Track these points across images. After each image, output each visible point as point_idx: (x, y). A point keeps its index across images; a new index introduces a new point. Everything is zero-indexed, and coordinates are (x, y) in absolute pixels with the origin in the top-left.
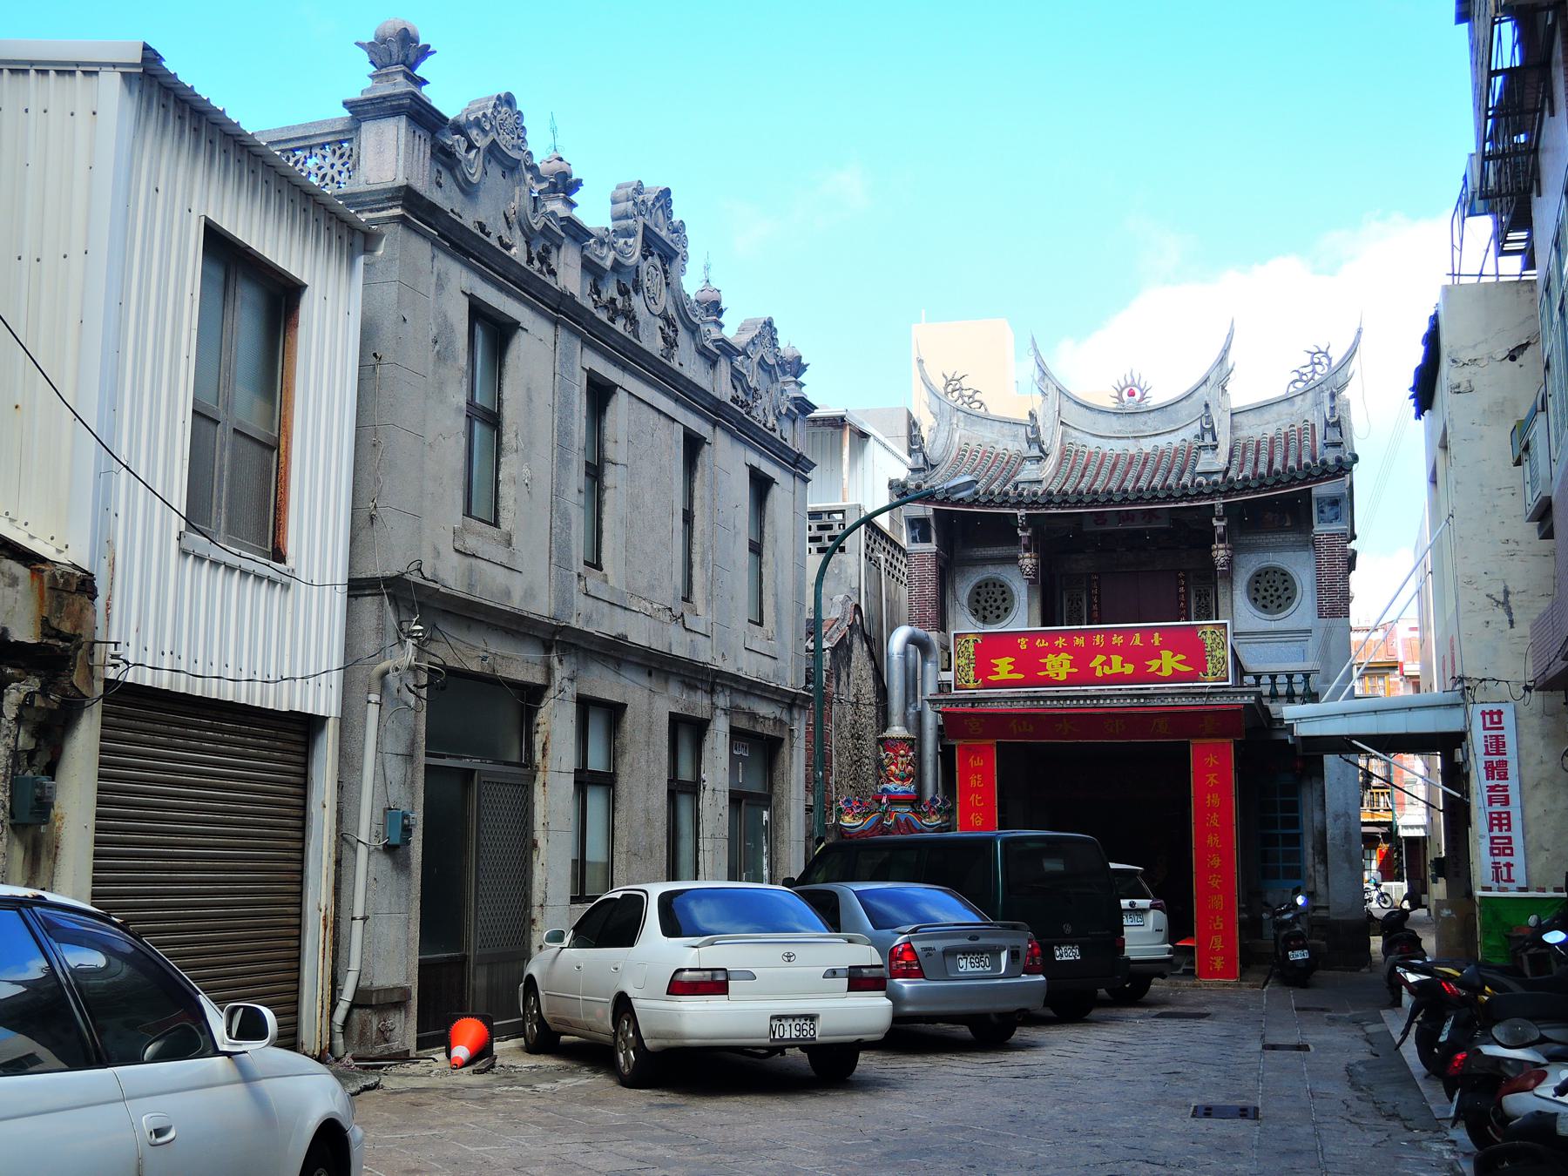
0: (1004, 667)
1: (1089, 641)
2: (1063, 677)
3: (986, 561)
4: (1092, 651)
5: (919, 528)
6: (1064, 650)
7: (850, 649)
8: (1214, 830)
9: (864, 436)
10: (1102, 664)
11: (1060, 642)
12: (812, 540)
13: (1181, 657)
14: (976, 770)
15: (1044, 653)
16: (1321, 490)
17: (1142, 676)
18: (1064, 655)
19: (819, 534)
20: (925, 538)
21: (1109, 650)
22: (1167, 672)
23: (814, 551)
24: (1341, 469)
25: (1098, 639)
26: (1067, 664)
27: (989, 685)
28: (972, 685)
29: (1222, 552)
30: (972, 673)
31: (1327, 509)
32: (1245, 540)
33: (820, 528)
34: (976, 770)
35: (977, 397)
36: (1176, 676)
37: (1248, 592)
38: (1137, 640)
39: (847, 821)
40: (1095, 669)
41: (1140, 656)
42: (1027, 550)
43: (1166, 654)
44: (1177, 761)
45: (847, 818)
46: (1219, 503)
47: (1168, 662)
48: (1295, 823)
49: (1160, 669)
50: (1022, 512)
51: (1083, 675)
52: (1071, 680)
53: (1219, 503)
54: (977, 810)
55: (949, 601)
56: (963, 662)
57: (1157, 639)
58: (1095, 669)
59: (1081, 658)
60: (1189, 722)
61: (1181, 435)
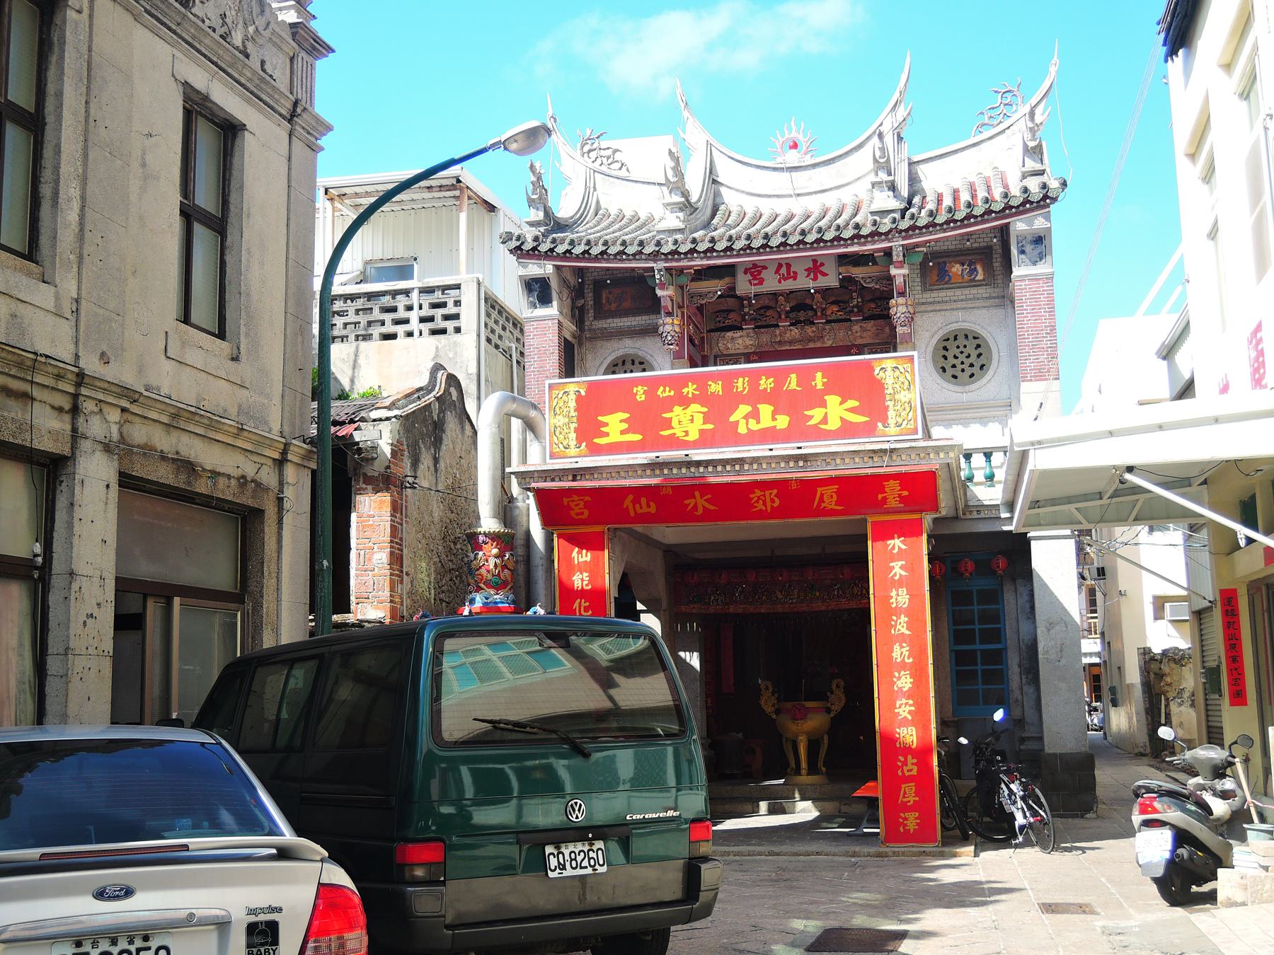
0: (615, 425)
2: (693, 436)
3: (622, 333)
4: (731, 400)
5: (538, 290)
6: (695, 399)
10: (746, 417)
11: (690, 390)
13: (852, 403)
15: (668, 404)
16: (1019, 226)
17: (799, 430)
20: (545, 300)
21: (755, 397)
22: (833, 424)
24: (1045, 197)
25: (741, 384)
26: (699, 418)
27: (595, 450)
29: (902, 309)
30: (573, 435)
33: (435, 306)
35: (618, 156)
36: (847, 430)
37: (935, 361)
38: (793, 382)
41: (796, 405)
43: (833, 400)
44: (853, 565)
47: (836, 410)
48: (996, 636)
49: (825, 420)
50: (662, 265)
51: (721, 432)
52: (705, 440)
53: (897, 244)
56: (560, 420)
57: (819, 381)
59: (718, 410)
60: (860, 491)
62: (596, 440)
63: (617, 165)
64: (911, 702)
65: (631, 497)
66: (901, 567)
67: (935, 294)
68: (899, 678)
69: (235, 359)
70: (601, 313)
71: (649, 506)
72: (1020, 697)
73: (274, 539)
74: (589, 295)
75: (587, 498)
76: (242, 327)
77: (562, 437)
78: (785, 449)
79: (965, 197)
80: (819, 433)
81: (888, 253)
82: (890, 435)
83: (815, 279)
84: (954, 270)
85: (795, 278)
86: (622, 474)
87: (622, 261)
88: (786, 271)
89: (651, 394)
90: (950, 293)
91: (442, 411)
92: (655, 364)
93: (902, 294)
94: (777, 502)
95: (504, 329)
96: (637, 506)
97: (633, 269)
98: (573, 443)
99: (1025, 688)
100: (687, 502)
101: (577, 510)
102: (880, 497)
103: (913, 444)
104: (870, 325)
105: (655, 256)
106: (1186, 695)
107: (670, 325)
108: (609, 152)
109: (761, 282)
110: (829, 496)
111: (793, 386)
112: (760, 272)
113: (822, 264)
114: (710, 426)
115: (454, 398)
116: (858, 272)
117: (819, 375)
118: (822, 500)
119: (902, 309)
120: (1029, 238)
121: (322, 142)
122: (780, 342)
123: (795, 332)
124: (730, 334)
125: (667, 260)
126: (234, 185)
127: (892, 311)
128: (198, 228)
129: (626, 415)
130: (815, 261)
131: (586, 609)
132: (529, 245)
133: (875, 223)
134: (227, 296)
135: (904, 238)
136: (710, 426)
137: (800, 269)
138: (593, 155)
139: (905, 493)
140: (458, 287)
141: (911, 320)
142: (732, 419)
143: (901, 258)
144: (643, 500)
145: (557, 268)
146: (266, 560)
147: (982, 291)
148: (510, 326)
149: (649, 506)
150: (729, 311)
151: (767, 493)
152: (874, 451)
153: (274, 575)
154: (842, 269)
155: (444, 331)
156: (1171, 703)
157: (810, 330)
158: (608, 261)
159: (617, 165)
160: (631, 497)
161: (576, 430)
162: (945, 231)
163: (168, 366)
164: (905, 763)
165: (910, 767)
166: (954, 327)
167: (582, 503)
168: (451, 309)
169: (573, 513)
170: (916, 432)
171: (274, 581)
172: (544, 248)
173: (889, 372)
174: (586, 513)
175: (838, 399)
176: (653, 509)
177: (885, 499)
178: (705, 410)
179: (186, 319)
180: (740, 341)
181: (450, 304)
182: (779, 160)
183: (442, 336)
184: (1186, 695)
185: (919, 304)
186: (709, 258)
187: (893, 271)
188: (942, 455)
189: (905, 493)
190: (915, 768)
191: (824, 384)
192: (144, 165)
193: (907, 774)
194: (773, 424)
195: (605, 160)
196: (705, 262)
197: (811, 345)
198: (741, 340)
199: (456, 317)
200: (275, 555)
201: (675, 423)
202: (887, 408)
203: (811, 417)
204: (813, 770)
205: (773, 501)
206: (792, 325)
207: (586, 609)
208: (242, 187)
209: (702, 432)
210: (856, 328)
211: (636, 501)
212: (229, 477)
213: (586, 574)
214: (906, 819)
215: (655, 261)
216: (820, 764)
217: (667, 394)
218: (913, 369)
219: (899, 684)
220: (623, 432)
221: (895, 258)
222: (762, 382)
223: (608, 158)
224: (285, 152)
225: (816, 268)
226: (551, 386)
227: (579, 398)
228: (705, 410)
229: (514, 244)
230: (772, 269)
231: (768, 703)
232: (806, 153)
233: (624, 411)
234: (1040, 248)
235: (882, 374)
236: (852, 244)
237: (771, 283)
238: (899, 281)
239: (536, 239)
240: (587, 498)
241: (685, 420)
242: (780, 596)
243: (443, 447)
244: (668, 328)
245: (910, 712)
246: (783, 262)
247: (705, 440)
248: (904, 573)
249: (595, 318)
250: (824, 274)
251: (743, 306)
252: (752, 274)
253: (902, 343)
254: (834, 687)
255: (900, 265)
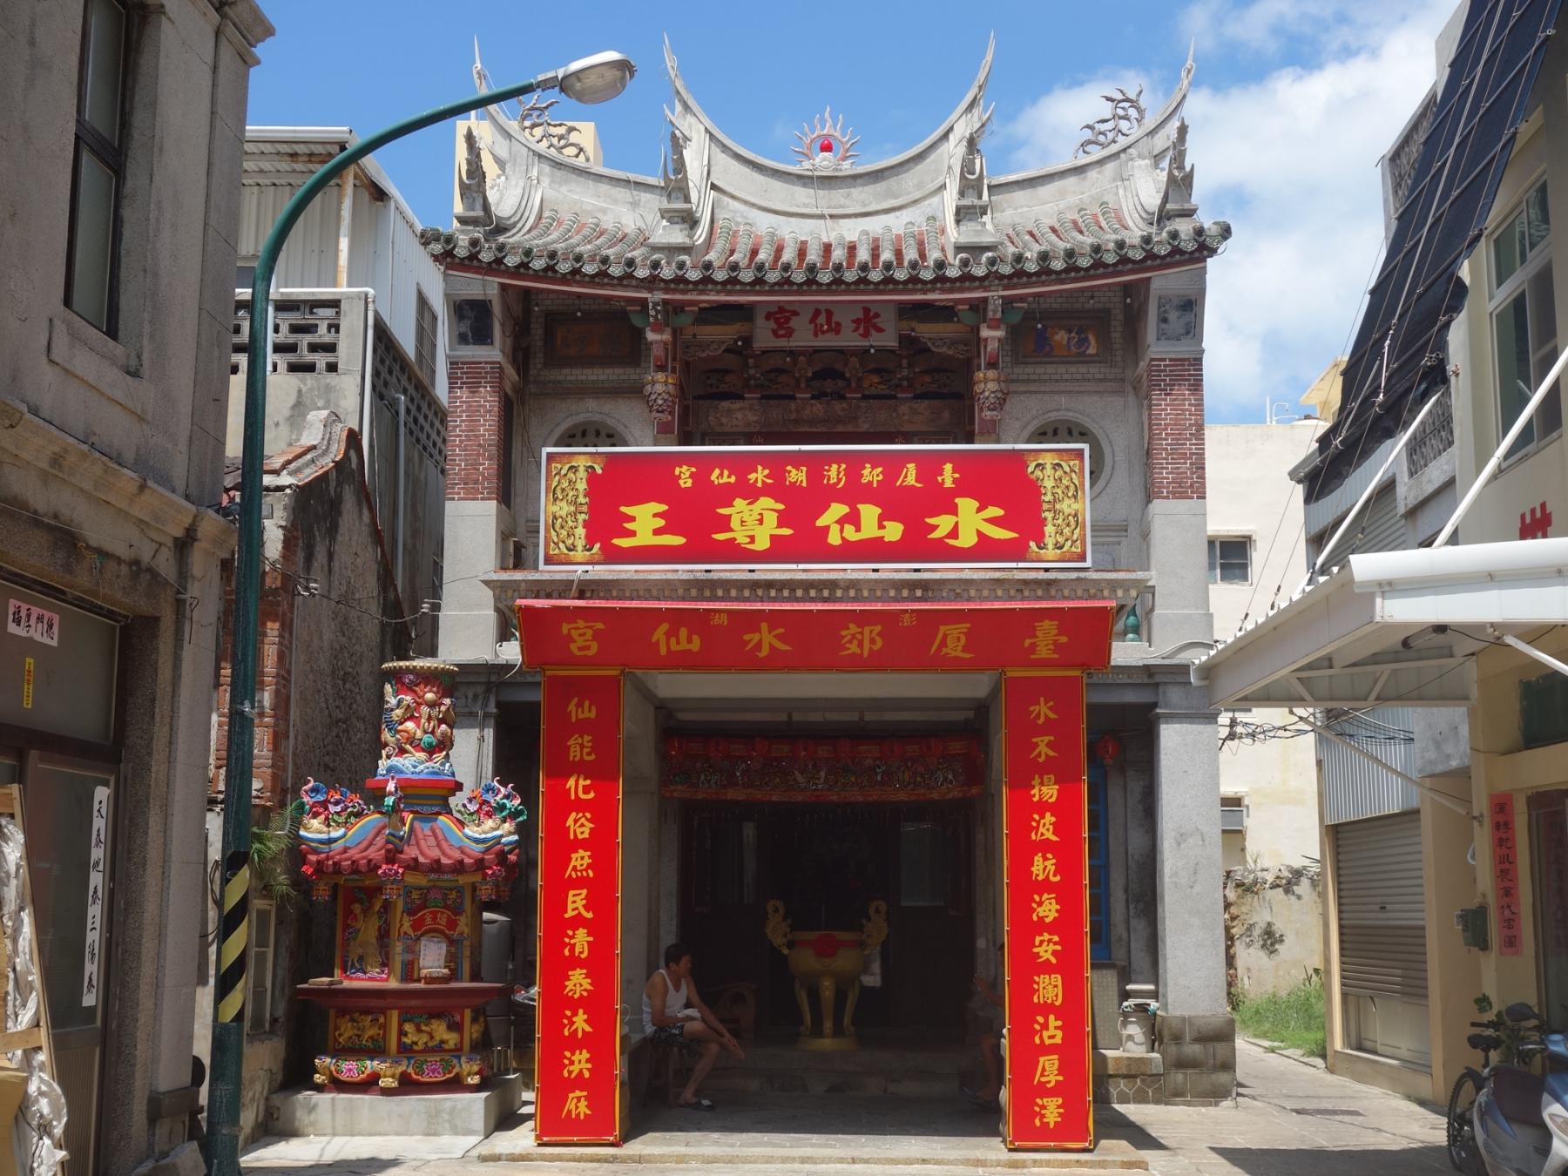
0: (645, 521)
1: (816, 474)
2: (762, 544)
4: (820, 496)
6: (766, 491)
7: (335, 506)
8: (1045, 847)
9: (380, 195)
10: (841, 522)
11: (759, 476)
12: (278, 348)
13: (995, 512)
14: (583, 727)
15: (727, 495)
16: (1164, 283)
17: (918, 545)
18: (766, 502)
19: (292, 338)
20: (480, 335)
21: (854, 494)
22: (967, 540)
23: (282, 367)
25: (834, 473)
26: (771, 519)
27: (614, 556)
28: (580, 554)
29: (992, 386)
30: (581, 531)
31: (1173, 316)
32: (1022, 371)
33: (295, 329)
34: (583, 727)
35: (573, 137)
36: (985, 549)
38: (910, 476)
39: (314, 829)
40: (826, 529)
41: (915, 508)
42: (661, 368)
43: (967, 505)
45: (315, 823)
46: (995, 295)
47: (970, 521)
49: (954, 533)
50: (659, 296)
51: (802, 541)
52: (779, 551)
53: (995, 295)
54: (580, 806)
55: (515, 456)
56: (563, 508)
57: (948, 476)
58: (826, 529)
59: (800, 509)
61: (905, 216)
62: (616, 541)
63: (572, 151)
64: (1056, 938)
65: (665, 627)
66: (1049, 745)
67: (1029, 370)
68: (1040, 904)
69: (134, 374)
70: (555, 359)
71: (689, 641)
72: (1125, 935)
73: (169, 665)
74: (537, 331)
75: (600, 626)
76: (146, 324)
77: (564, 533)
78: (897, 571)
79: (911, 254)
80: (944, 551)
81: (979, 307)
82: (1045, 561)
83: (866, 335)
84: (1057, 337)
85: (837, 332)
86: (733, 593)
87: (602, 286)
88: (825, 318)
89: (701, 478)
90: (1050, 369)
91: (339, 484)
92: (629, 438)
93: (992, 365)
94: (879, 643)
95: (390, 372)
96: (673, 641)
97: (609, 298)
98: (580, 544)
99: (1134, 922)
100: (747, 637)
101: (580, 642)
102: (1027, 642)
103: (1082, 575)
104: (923, 406)
105: (652, 282)
106: (1257, 932)
107: (661, 385)
108: (562, 130)
109: (790, 333)
110: (954, 639)
111: (911, 479)
112: (788, 320)
113: (877, 315)
114: (787, 532)
115: (354, 465)
116: (926, 331)
117: (948, 467)
118: (943, 643)
119: (992, 386)
120: (1175, 302)
121: (260, 50)
122: (797, 422)
123: (818, 408)
124: (725, 404)
125: (666, 291)
126: (140, 98)
127: (978, 388)
128: (86, 157)
129: (663, 508)
130: (866, 310)
131: (586, 790)
132: (461, 252)
133: (965, 263)
134: (123, 274)
135: (1006, 288)
136: (787, 532)
137: (845, 318)
138: (538, 132)
139: (1064, 639)
140: (335, 304)
141: (1000, 403)
142: (820, 522)
143: (999, 315)
144: (683, 632)
145: (503, 287)
146: (159, 696)
147: (1094, 370)
148: (396, 368)
149: (689, 641)
150: (727, 372)
151: (867, 630)
152: (1025, 582)
153: (167, 720)
154: (905, 324)
155: (310, 368)
156: (1237, 943)
157: (839, 407)
158: (581, 284)
159: (572, 151)
160: (665, 627)
161: (586, 524)
162: (1062, 282)
163: (49, 374)
164: (1045, 1026)
165: (1052, 1031)
166: (1054, 416)
167: (589, 633)
168: (323, 335)
169: (573, 647)
170: (1082, 558)
171: (166, 729)
172: (486, 257)
173: (1049, 470)
174: (594, 647)
175: (976, 504)
176: (696, 645)
177: (1033, 647)
178: (781, 507)
179: (67, 302)
180: (739, 415)
181: (323, 329)
182: (807, 164)
183: (308, 375)
184: (1257, 932)
185: (1013, 381)
186: (729, 293)
187: (985, 333)
188: (1120, 593)
189: (1064, 639)
190: (1059, 1034)
191: (955, 481)
192: (32, 43)
193: (1048, 1042)
194: (879, 533)
195: (555, 141)
196: (723, 298)
197: (840, 429)
198: (740, 414)
199: (331, 348)
200: (169, 689)
201: (735, 523)
202: (1043, 522)
203: (935, 527)
204: (838, 1032)
205: (873, 641)
206: (813, 397)
207: (586, 790)
208: (153, 104)
209: (774, 538)
210: (904, 408)
211: (672, 633)
212: (119, 560)
213: (587, 738)
214: (1043, 1107)
215: (651, 290)
216: (847, 1020)
217: (725, 480)
218: (1082, 469)
219: (1041, 911)
220: (657, 532)
221: (990, 314)
222: (866, 472)
223: (561, 138)
224: (209, 58)
225: (867, 320)
226: (550, 456)
227: (592, 478)
228: (781, 507)
229: (437, 248)
230: (807, 315)
231: (776, 931)
232: (845, 158)
233: (659, 501)
234: (1188, 317)
235: (1038, 473)
236: (933, 290)
237: (803, 337)
238: (992, 346)
239: (474, 243)
240: (600, 626)
241: (751, 519)
242: (800, 778)
243: (339, 538)
244: (659, 388)
245: (1054, 953)
246: (822, 308)
247: (779, 551)
248: (1052, 753)
249: (546, 365)
250: (880, 330)
251: (747, 366)
252: (777, 321)
253: (981, 433)
254: (872, 912)
255: (994, 326)
